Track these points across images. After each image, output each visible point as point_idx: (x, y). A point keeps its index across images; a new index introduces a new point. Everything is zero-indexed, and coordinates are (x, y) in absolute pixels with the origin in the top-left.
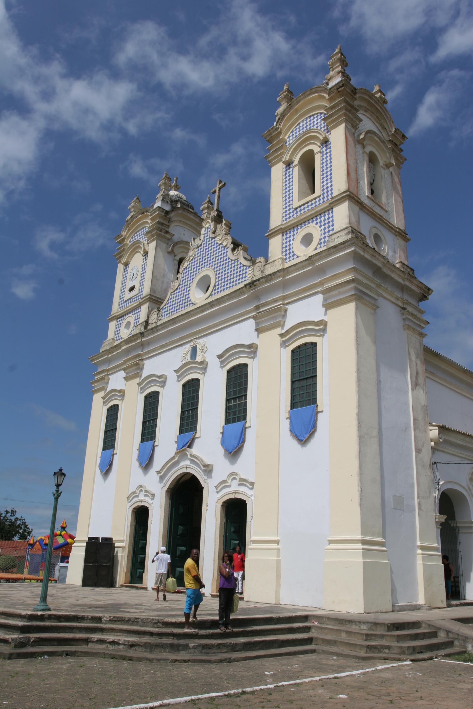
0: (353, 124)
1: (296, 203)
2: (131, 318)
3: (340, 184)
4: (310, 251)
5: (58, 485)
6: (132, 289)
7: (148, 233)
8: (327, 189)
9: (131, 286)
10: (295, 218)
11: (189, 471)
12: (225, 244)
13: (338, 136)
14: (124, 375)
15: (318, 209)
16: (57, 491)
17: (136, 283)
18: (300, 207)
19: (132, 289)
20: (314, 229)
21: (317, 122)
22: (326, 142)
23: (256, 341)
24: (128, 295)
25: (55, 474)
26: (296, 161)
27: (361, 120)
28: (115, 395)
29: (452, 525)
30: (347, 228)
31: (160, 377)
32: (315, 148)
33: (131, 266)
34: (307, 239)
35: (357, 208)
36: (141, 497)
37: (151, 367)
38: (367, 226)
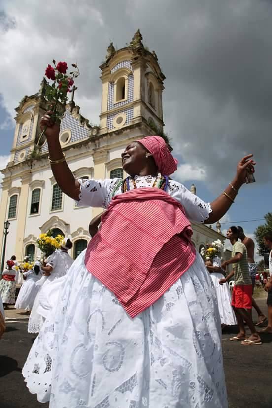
0: (144, 68)
1: (115, 102)
2: (24, 152)
3: (137, 96)
4: (215, 229)
5: (7, 228)
6: (24, 137)
7: (35, 108)
8: (131, 97)
9: (24, 135)
10: (113, 109)
11: (57, 227)
12: (77, 118)
13: (137, 73)
14: (21, 180)
15: (127, 106)
16: (6, 231)
17: (27, 134)
18: (117, 104)
19: (24, 137)
20: (124, 116)
21: (127, 65)
22: (131, 75)
23: (93, 166)
24: (22, 140)
25: (5, 223)
26: (116, 82)
27: (148, 67)
28: (15, 190)
29: (188, 279)
30: (140, 117)
31: (41, 181)
32: (126, 77)
33: (24, 125)
34: (120, 121)
35: (144, 108)
36: (31, 240)
37: (35, 177)
38: (148, 116)
